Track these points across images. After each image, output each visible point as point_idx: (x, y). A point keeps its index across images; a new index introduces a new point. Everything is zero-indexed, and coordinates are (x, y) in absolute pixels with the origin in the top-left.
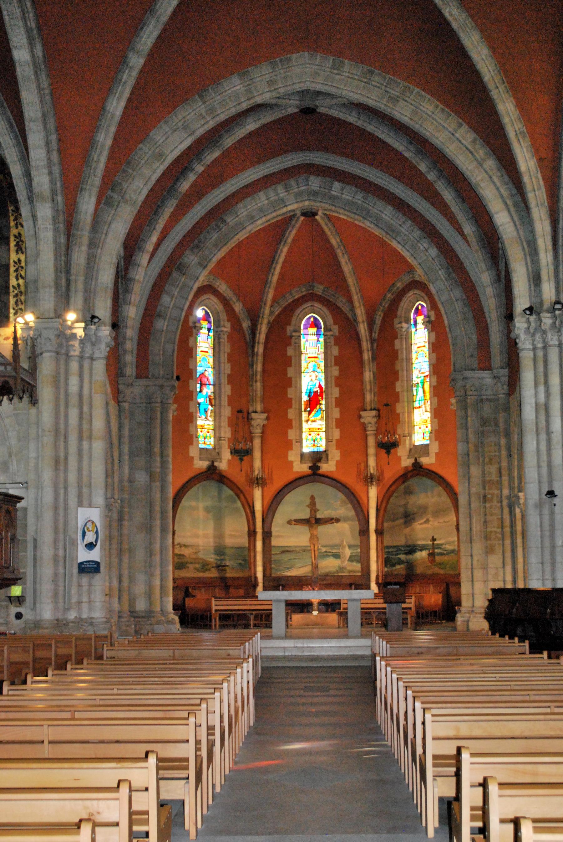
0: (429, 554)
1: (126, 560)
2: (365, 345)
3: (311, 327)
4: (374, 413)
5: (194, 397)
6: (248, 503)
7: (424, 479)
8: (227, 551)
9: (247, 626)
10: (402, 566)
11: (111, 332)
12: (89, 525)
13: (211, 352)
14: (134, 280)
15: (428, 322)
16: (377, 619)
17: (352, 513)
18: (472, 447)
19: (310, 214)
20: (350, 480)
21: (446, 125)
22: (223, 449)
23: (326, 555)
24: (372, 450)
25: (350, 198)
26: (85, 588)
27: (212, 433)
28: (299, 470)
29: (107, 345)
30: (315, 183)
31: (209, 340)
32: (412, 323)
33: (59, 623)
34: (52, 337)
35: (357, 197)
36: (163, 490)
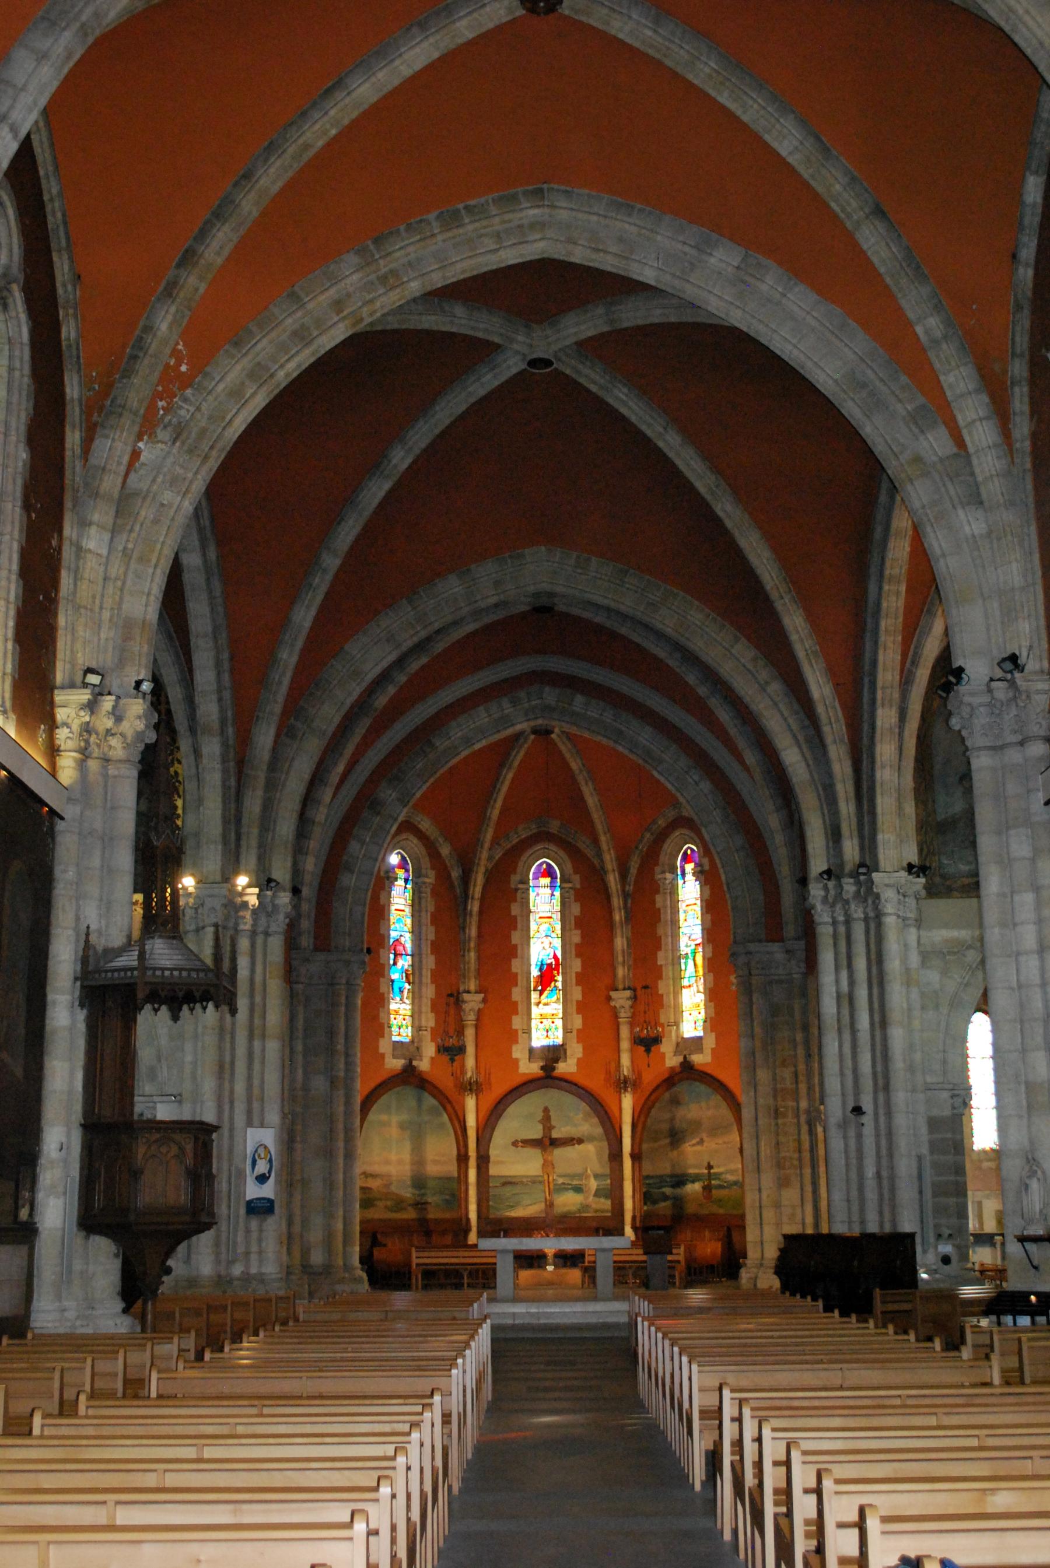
0: (704, 1188)
1: (297, 1197)
2: (616, 902)
4: (628, 993)
7: (698, 1083)
8: (431, 1184)
9: (458, 1286)
11: (292, 899)
12: (261, 1151)
13: (408, 910)
14: (314, 822)
16: (635, 1276)
17: (599, 1130)
18: (758, 1044)
19: (542, 733)
20: (595, 1083)
21: (719, 639)
23: (562, 1189)
24: (625, 1045)
26: (255, 1235)
27: (409, 1020)
28: (527, 1072)
29: (287, 916)
30: (550, 695)
31: (407, 894)
32: (679, 873)
33: (222, 1281)
34: (218, 907)
35: (605, 714)
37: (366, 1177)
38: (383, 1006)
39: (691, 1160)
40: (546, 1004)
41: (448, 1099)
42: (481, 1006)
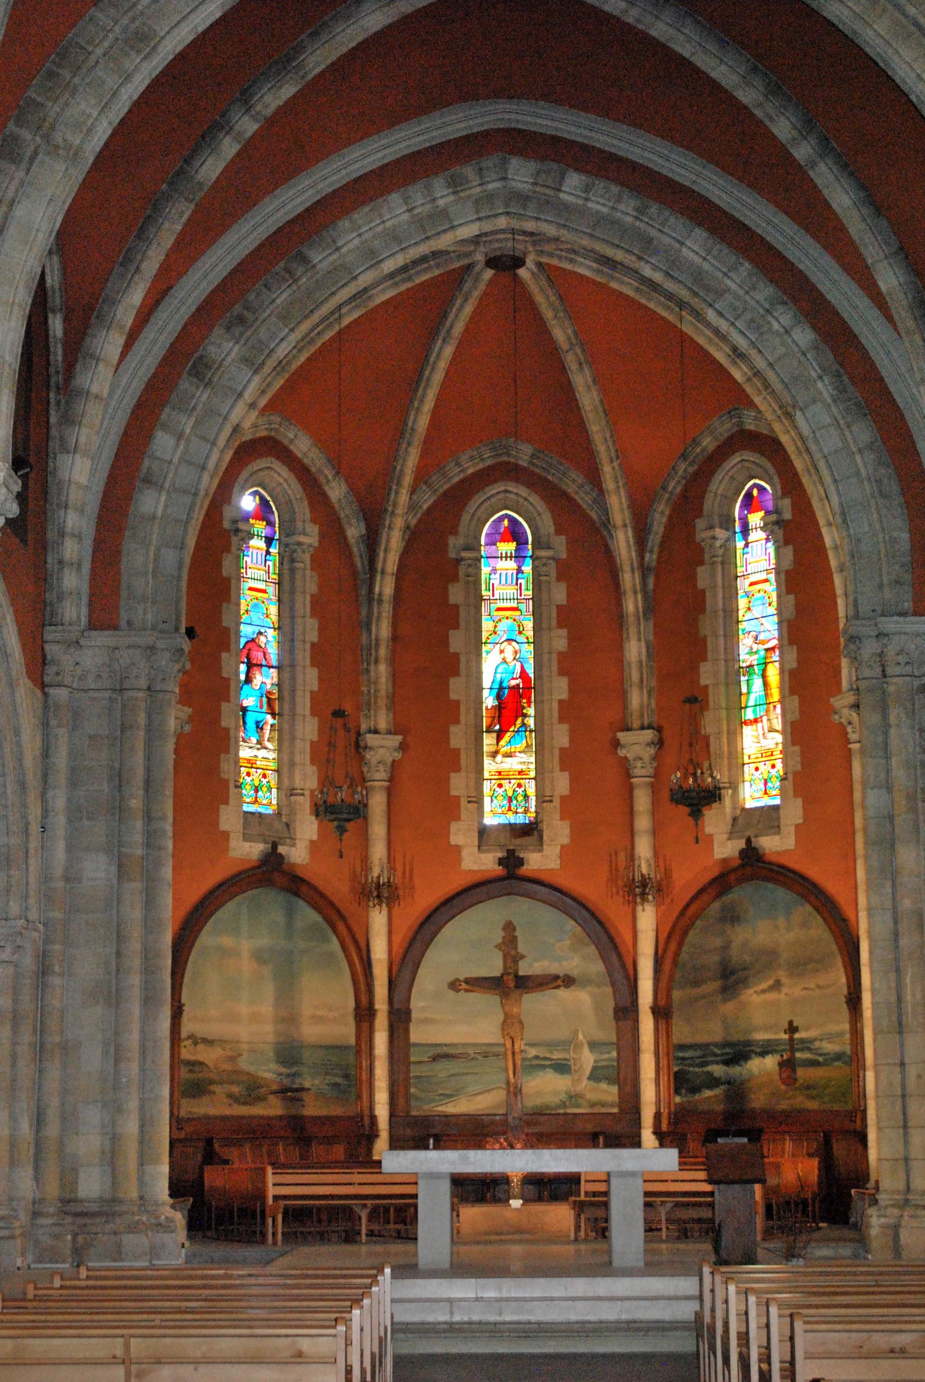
0: (781, 1065)
1: (54, 1074)
2: (629, 579)
3: (503, 540)
4: (649, 735)
5: (232, 693)
6: (356, 942)
7: (771, 886)
8: (306, 1054)
9: (350, 1237)
10: (717, 1091)
13: (272, 590)
14: (88, 392)
15: (777, 523)
17: (597, 967)
19: (506, 264)
20: (593, 888)
22: (298, 817)
23: (536, 1065)
25: (605, 210)
27: (272, 778)
28: (475, 868)
30: (521, 173)
35: (622, 207)
36: (150, 902)
37: (196, 1044)
38: (227, 751)
39: (758, 1018)
40: (508, 755)
41: (339, 912)
42: (398, 755)
